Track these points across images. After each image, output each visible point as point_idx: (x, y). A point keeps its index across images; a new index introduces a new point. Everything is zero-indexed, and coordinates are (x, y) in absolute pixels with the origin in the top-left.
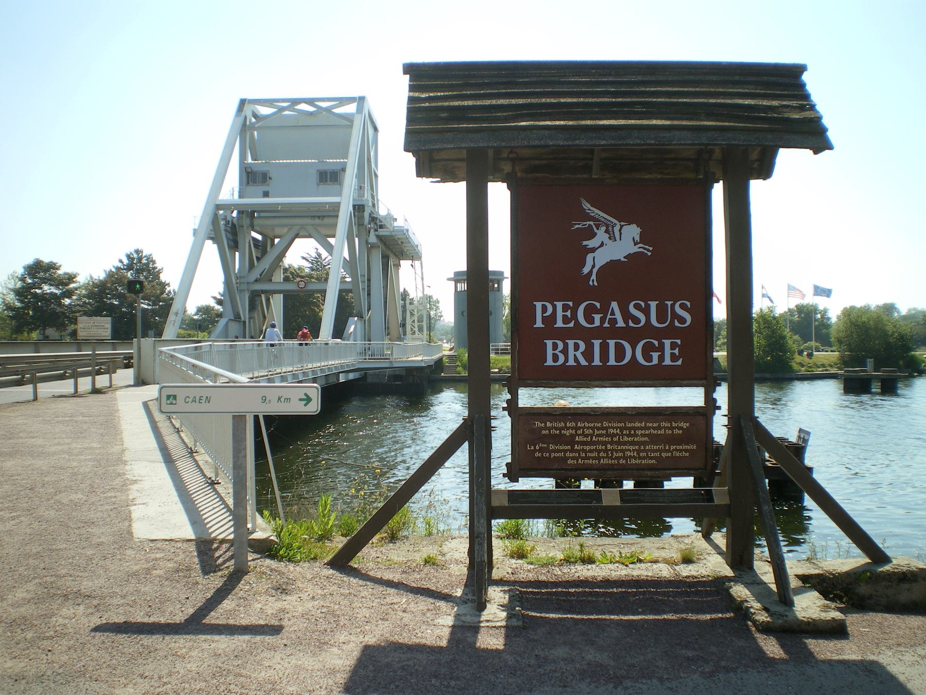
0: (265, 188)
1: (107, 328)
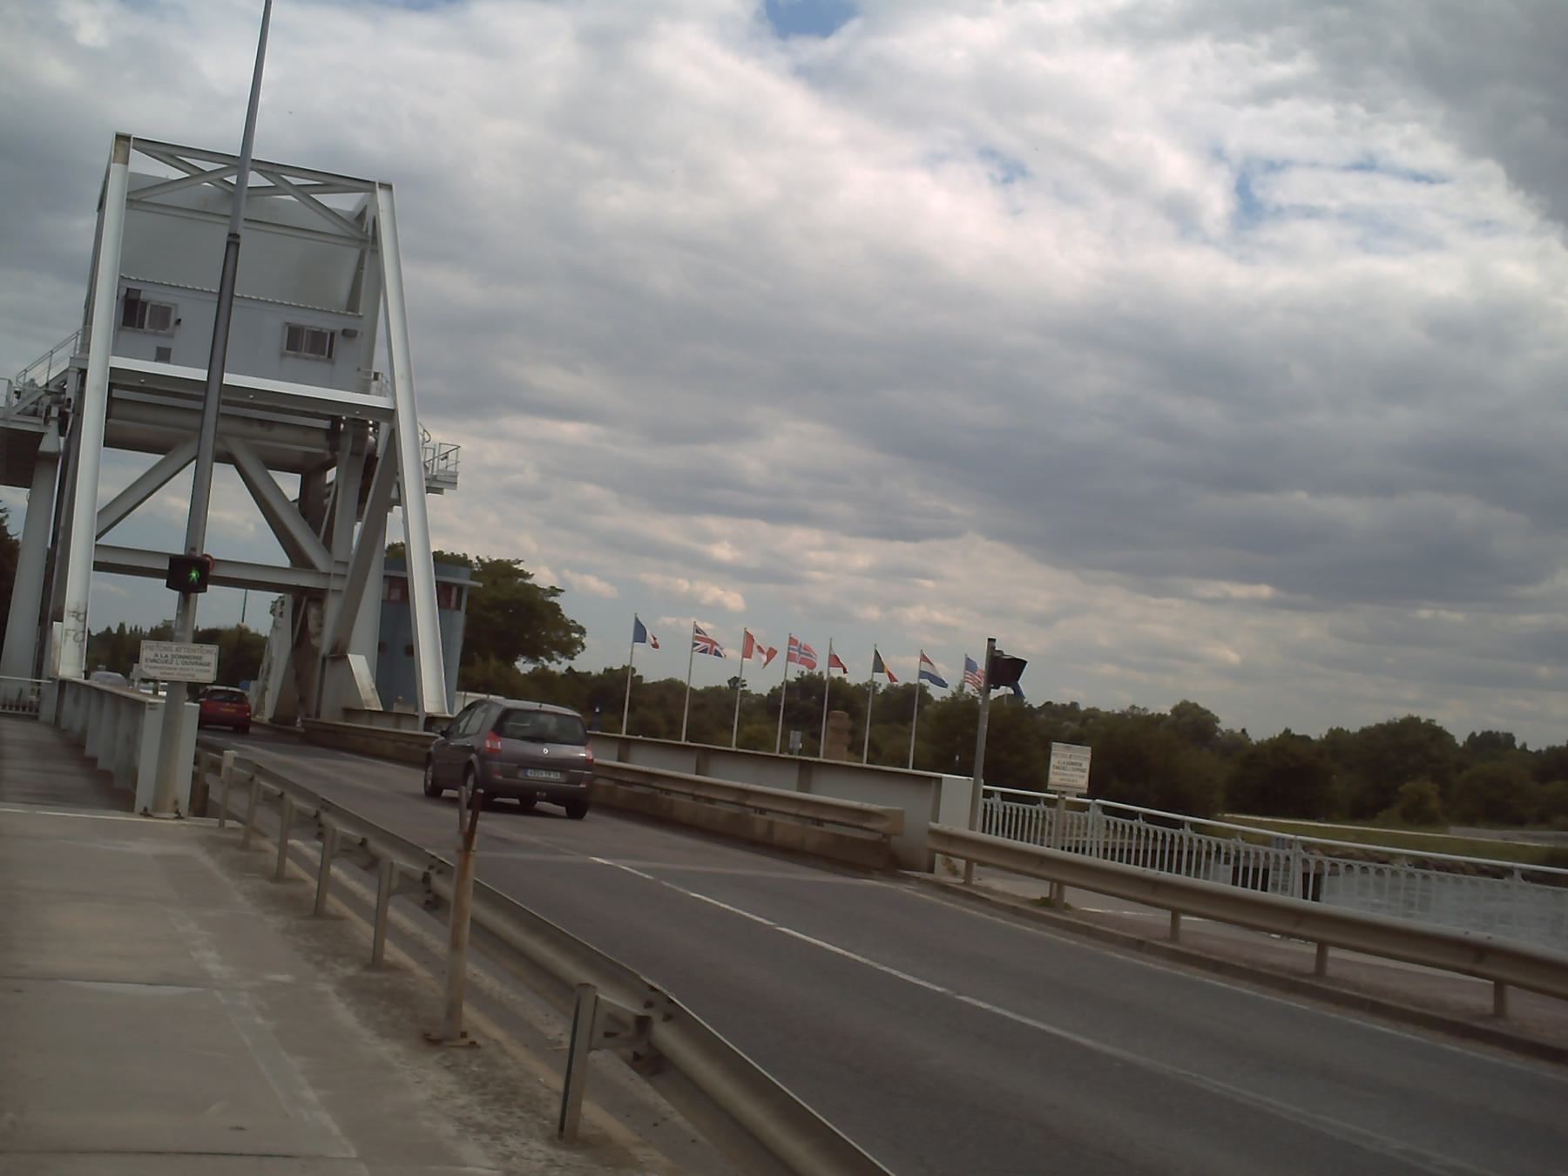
0: (165, 343)
1: (208, 664)
